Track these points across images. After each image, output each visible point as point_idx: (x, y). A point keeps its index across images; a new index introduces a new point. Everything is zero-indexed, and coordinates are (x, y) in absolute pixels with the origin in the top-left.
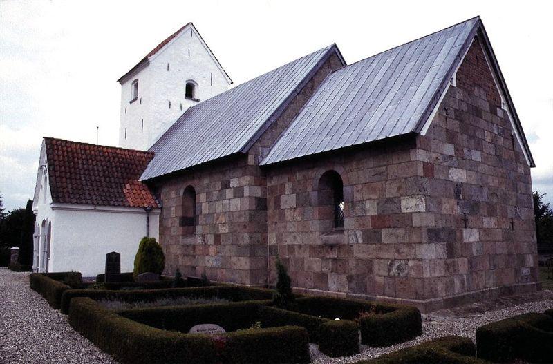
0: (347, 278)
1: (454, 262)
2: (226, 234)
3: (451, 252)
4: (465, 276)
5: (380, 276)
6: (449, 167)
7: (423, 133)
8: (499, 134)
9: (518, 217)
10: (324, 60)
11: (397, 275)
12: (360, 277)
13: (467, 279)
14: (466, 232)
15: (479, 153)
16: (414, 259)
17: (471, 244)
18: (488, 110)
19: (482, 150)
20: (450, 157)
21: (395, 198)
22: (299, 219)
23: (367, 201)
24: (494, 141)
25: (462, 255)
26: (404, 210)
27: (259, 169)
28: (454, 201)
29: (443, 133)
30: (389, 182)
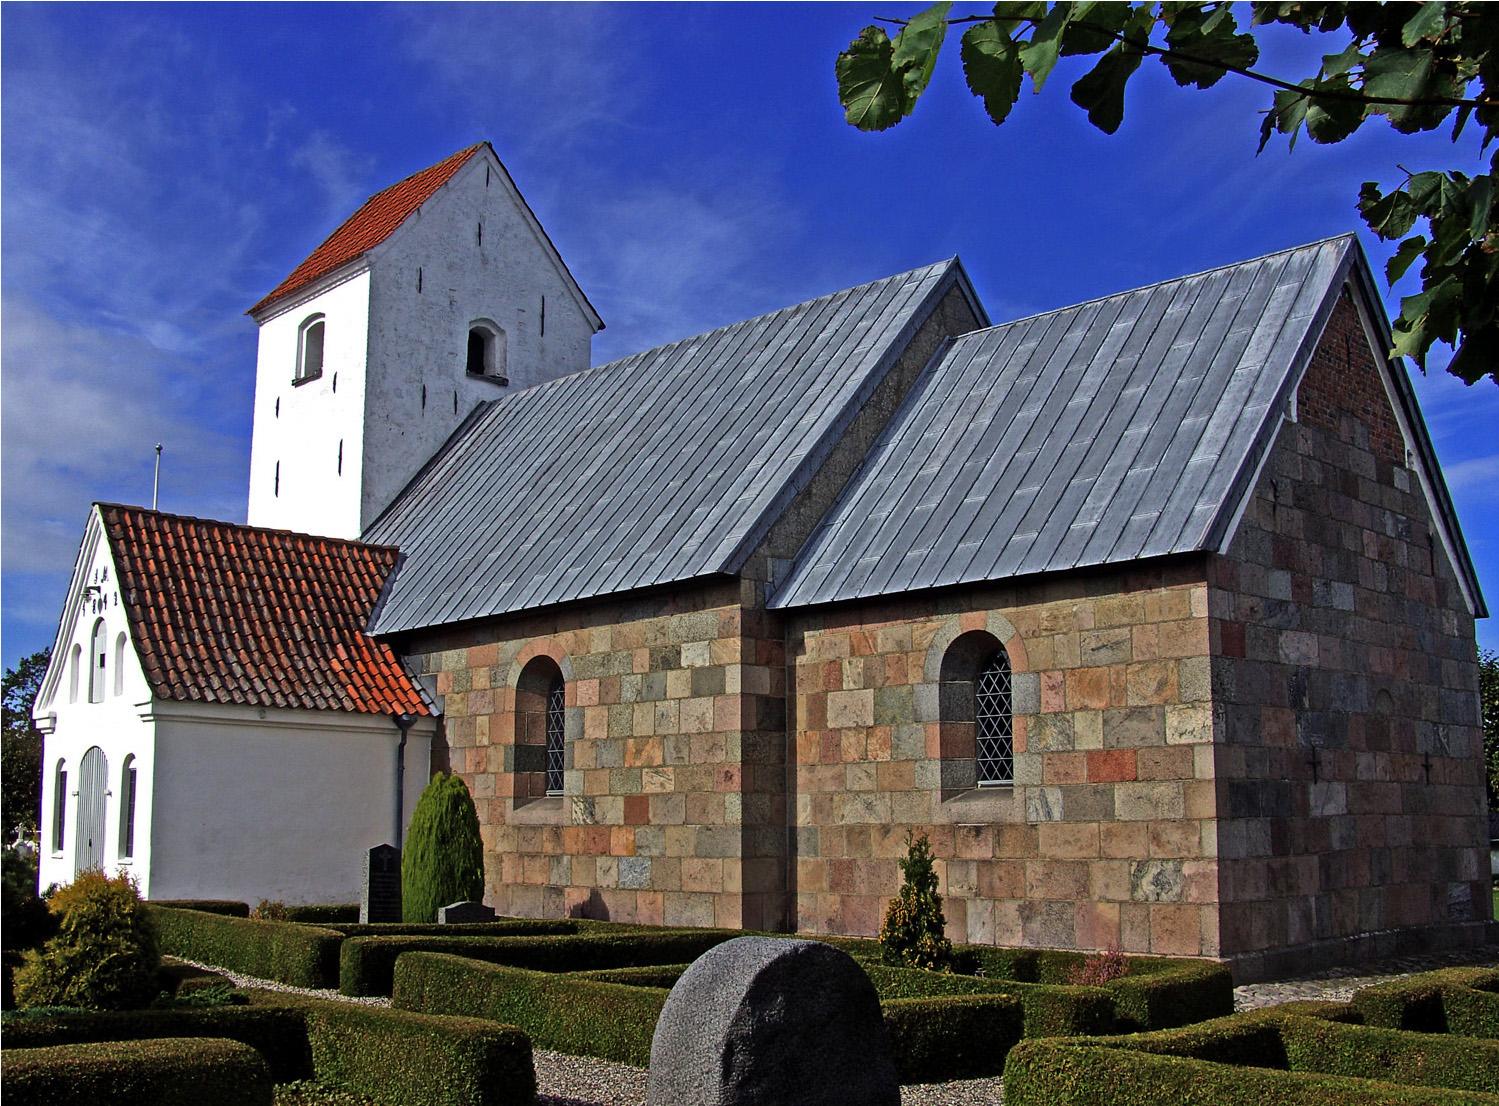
0: (1021, 910)
1: (1287, 865)
2: (666, 797)
3: (1280, 841)
4: (1313, 900)
5: (1108, 901)
6: (1280, 630)
7: (1224, 550)
8: (1399, 537)
9: (1441, 751)
10: (930, 309)
11: (1152, 898)
12: (1056, 907)
13: (1318, 911)
14: (1314, 790)
15: (1349, 588)
16: (1196, 859)
17: (1326, 820)
18: (1372, 474)
19: (1356, 583)
20: (1281, 603)
21: (1150, 707)
22: (885, 756)
23: (1078, 715)
24: (1386, 556)
25: (1307, 850)
26: (1172, 739)
27: (766, 620)
28: (1289, 715)
29: (1267, 546)
30: (1137, 667)
